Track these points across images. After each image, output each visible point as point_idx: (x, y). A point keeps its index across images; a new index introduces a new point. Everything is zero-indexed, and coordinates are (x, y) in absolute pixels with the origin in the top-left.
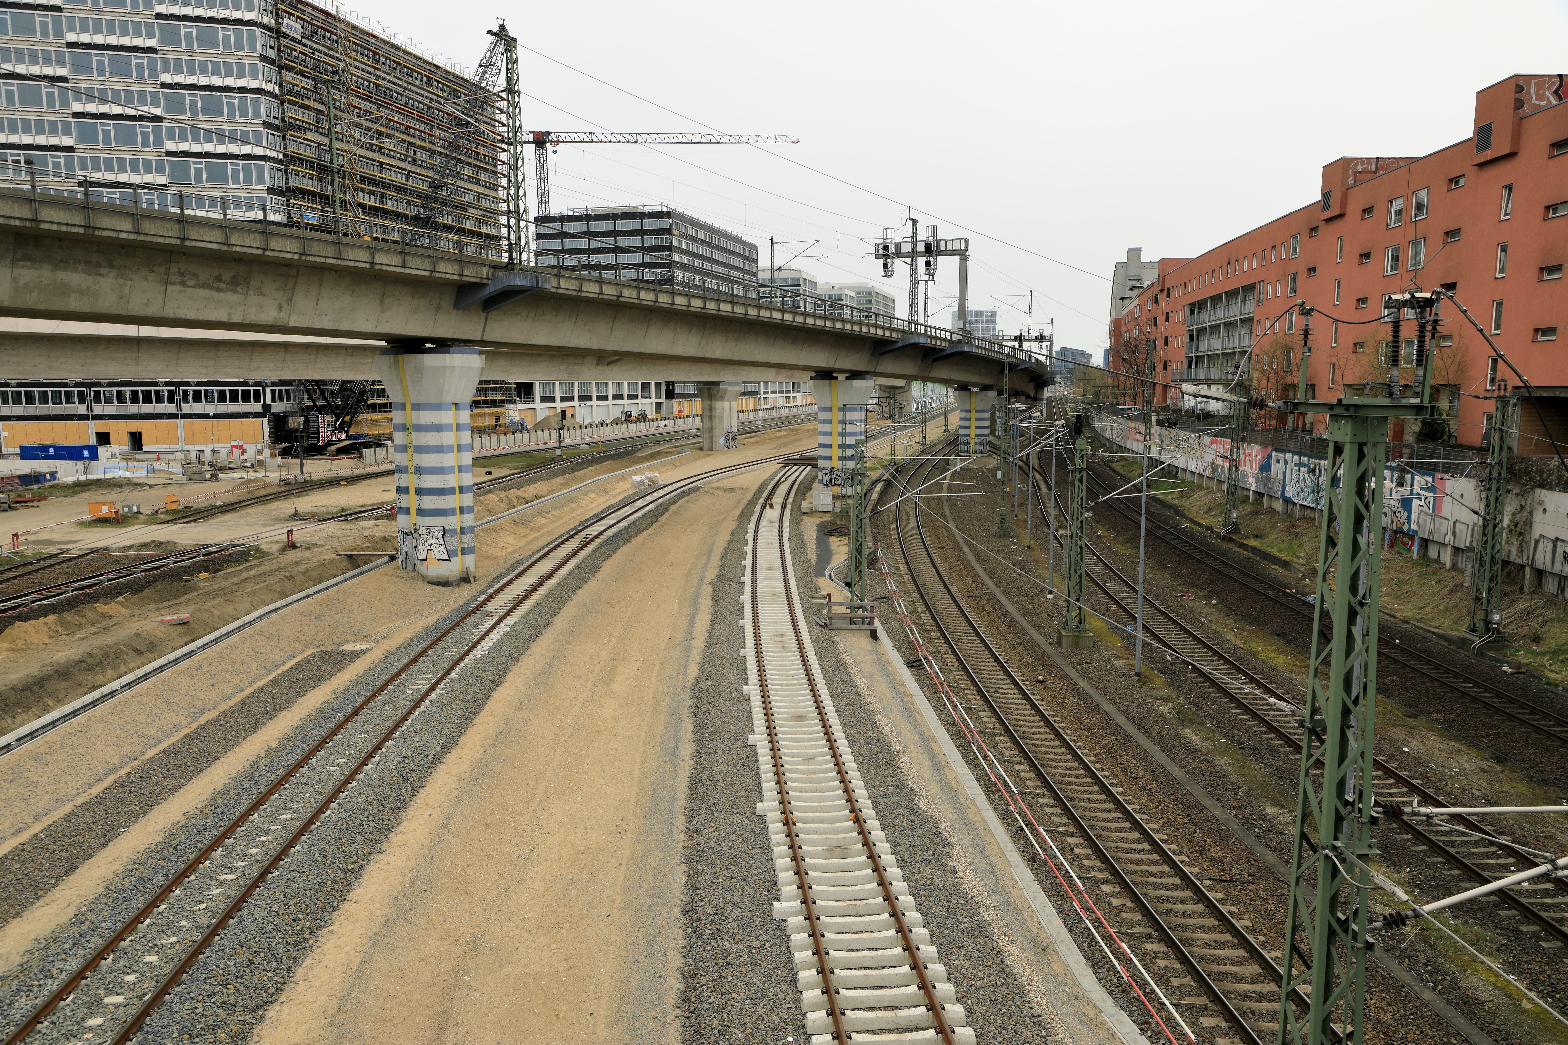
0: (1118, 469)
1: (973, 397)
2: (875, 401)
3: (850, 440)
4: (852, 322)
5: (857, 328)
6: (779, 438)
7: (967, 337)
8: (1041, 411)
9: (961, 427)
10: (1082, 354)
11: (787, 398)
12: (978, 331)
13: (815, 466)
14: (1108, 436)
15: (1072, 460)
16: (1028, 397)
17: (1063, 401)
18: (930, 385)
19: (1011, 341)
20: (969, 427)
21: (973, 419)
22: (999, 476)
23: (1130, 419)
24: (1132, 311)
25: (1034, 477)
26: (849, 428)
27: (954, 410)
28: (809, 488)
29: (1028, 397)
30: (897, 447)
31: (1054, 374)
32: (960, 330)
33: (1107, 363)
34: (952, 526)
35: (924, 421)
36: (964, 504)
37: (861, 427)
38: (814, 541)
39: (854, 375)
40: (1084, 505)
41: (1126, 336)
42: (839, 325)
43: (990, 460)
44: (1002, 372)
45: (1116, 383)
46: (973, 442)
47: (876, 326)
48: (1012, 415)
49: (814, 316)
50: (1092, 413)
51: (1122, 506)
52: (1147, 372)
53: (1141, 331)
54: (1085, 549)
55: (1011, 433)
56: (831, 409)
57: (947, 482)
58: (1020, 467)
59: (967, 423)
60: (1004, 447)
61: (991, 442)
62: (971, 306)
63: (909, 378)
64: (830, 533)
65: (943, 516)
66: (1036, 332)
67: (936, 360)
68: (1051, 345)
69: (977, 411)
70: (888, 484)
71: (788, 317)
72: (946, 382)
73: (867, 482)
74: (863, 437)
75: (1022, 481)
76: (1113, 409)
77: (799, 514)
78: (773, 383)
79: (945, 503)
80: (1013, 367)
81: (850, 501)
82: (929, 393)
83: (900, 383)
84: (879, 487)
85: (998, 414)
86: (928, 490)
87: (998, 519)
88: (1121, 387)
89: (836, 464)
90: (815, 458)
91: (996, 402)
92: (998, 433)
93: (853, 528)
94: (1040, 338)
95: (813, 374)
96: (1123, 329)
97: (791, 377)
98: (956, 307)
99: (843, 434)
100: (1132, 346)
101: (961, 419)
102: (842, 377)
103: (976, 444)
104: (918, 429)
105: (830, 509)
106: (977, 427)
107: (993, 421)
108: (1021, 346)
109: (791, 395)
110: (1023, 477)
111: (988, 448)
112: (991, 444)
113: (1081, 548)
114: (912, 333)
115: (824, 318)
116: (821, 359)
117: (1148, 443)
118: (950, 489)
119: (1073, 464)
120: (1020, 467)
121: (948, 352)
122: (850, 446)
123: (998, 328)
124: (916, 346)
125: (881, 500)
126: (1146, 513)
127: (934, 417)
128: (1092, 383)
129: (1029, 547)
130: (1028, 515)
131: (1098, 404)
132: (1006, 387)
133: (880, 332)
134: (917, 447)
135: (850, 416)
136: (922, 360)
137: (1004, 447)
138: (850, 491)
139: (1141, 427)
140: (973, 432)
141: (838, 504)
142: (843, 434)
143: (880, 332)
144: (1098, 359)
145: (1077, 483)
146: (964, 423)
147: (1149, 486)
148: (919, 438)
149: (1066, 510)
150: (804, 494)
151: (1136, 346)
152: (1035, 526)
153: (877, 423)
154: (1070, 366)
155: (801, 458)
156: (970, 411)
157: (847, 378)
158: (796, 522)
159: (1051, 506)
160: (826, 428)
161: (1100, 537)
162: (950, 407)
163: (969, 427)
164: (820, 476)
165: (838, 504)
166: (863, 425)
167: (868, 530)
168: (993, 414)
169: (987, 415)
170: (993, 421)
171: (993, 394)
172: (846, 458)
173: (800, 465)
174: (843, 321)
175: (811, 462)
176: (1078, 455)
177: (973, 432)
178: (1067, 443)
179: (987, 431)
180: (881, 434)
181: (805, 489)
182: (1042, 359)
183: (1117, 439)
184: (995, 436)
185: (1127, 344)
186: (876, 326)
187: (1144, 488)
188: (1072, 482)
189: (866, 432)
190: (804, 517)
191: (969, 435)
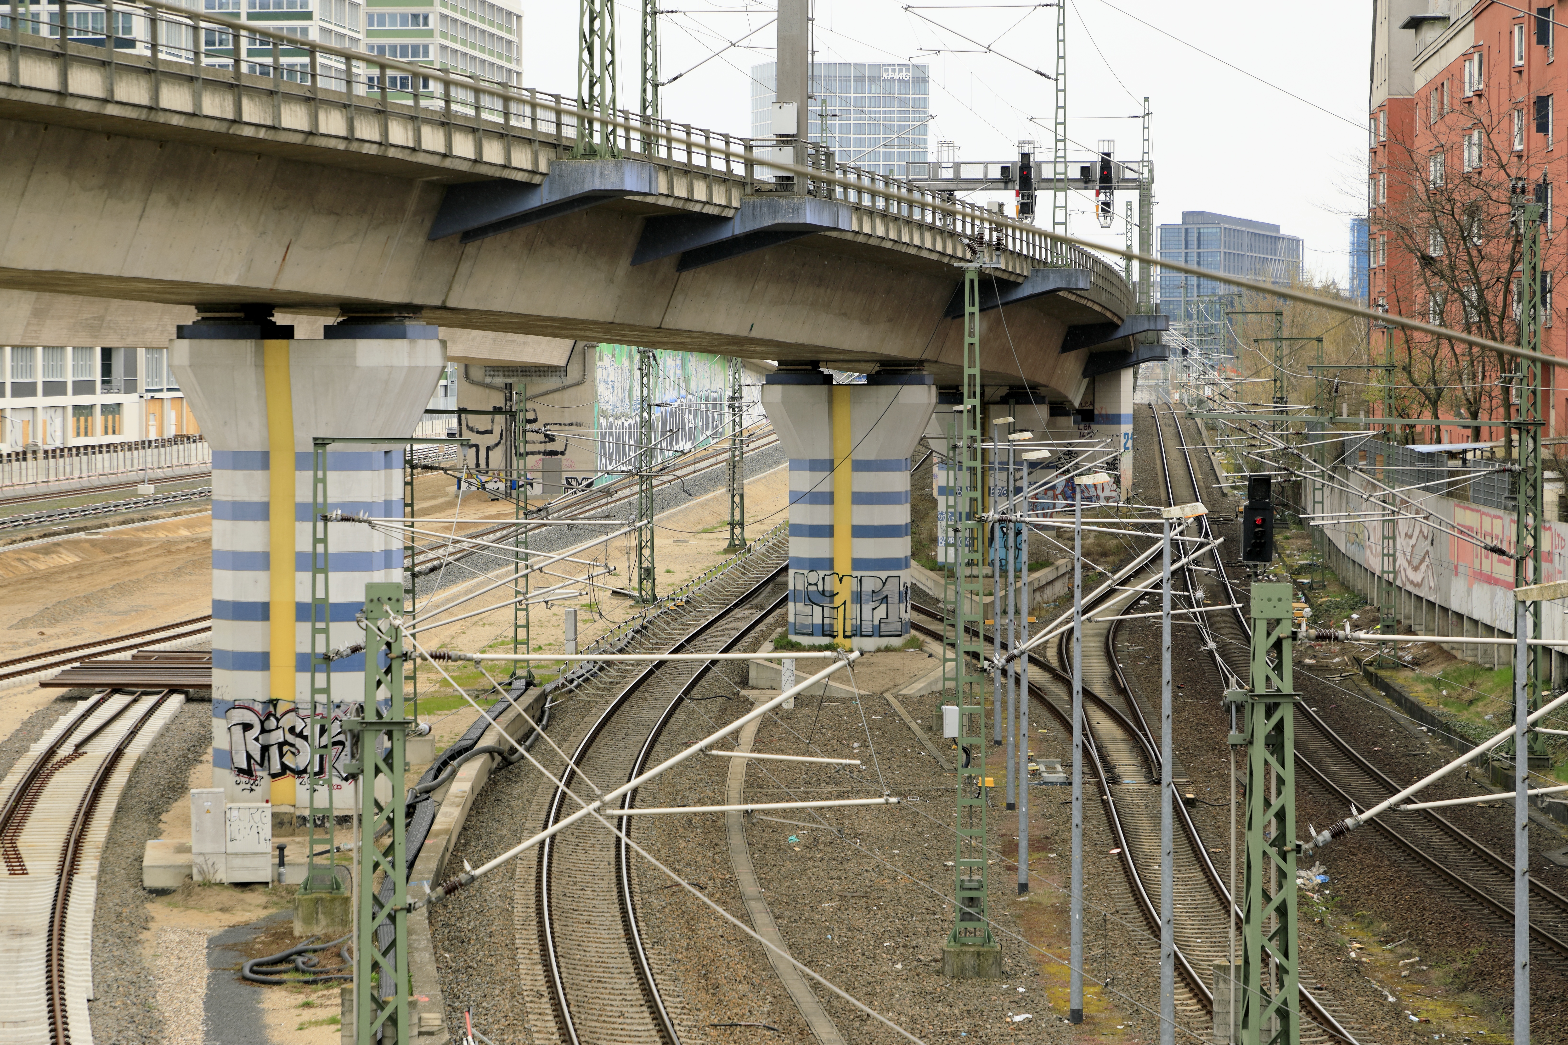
0: (1419, 693)
1: (842, 410)
2: (447, 424)
3: (346, 588)
4: (348, 106)
5: (367, 130)
6: (49, 577)
7: (812, 167)
8: (1113, 465)
9: (797, 530)
10: (1266, 240)
11: (79, 410)
12: (861, 148)
13: (197, 695)
14: (1375, 564)
15: (1239, 663)
16: (1059, 408)
17: (1195, 424)
18: (669, 361)
19: (987, 183)
20: (827, 531)
21: (843, 498)
22: (952, 719)
23: (1455, 493)
24: (1453, 73)
25: (1088, 730)
26: (342, 538)
27: (767, 460)
28: (177, 788)
29: (1059, 408)
30: (537, 612)
31: (1158, 318)
32: (784, 140)
33: (1364, 273)
34: (767, 937)
35: (647, 508)
36: (813, 843)
37: (389, 536)
38: (197, 1008)
39: (360, 319)
40: (1292, 840)
41: (1435, 171)
42: (294, 118)
43: (913, 662)
44: (955, 310)
45: (1400, 356)
46: (845, 591)
47: (447, 123)
48: (997, 480)
49: (189, 78)
50: (1311, 474)
51: (1438, 840)
52: (1517, 310)
53: (1489, 149)
54: (1298, 1018)
55: (997, 552)
56: (264, 460)
57: (741, 755)
58: (1035, 692)
59: (819, 515)
60: (968, 611)
61: (916, 591)
62: (828, 47)
63: (584, 333)
64: (264, 974)
65: (729, 892)
66: (1084, 152)
67: (690, 260)
68: (1146, 201)
69: (860, 466)
70: (504, 763)
71: (85, 82)
72: (732, 348)
73: (418, 757)
74: (398, 576)
75: (1044, 748)
76: (1395, 453)
77: (134, 896)
78: (23, 349)
79: (737, 840)
80: (994, 287)
81: (347, 840)
82: (666, 393)
83: (548, 351)
84: (468, 776)
85: (941, 477)
86: (668, 789)
87: (952, 903)
88: (1421, 369)
89: (294, 687)
90: (203, 661)
91: (934, 429)
92: (944, 554)
93: (361, 952)
94: (1102, 176)
95: (190, 316)
96: (1422, 143)
97: (95, 327)
98: (765, 49)
99: (317, 563)
100: (1459, 212)
101: (796, 498)
102: (308, 327)
103: (858, 597)
104: (622, 539)
105: (265, 874)
106: (860, 532)
107: (922, 505)
108: (1026, 208)
109: (99, 399)
110: (1051, 729)
111: (909, 615)
112: (920, 601)
113: (1283, 1014)
114: (591, 152)
115: (235, 87)
116: (227, 251)
117: (1530, 592)
118: (756, 784)
119: (1244, 679)
120: (1035, 692)
121: (737, 228)
122: (346, 612)
123: (935, 132)
124: (606, 205)
125: (471, 835)
126: (1535, 868)
127: (687, 491)
128: (1310, 352)
129: (1077, 1017)
130: (1074, 884)
131: (1331, 435)
132: (972, 370)
133: (463, 146)
134: (620, 613)
135: (345, 487)
136: (638, 259)
137: (968, 611)
138: (345, 798)
139: (1500, 526)
140: (845, 550)
141: (297, 852)
142: (317, 563)
143: (463, 146)
144: (1329, 261)
145: (1259, 753)
146: (806, 514)
147: (1539, 763)
148: (626, 576)
149: (1222, 863)
150: (155, 812)
151: (1472, 211)
152: (1099, 928)
153: (456, 516)
154: (1222, 289)
155: (141, 662)
156: (829, 466)
157: (330, 333)
158: (119, 931)
159: (1160, 845)
160: (248, 536)
161: (1356, 969)
162: (750, 450)
163: (827, 531)
164: (221, 735)
165: (298, 851)
166: (397, 523)
167: (424, 957)
168: (921, 472)
169: (899, 481)
170: (922, 505)
171: (920, 396)
172: (329, 661)
173: (137, 691)
174: (313, 101)
175: (186, 680)
176: (1261, 643)
177: (845, 550)
178: (1220, 593)
179: (900, 547)
180: (471, 560)
181: (157, 793)
182: (1114, 261)
183: (1411, 577)
184: (934, 566)
185: (1438, 201)
186: (447, 123)
187: (1522, 769)
188: (1242, 750)
189: (411, 551)
190: (156, 909)
191: (829, 564)
